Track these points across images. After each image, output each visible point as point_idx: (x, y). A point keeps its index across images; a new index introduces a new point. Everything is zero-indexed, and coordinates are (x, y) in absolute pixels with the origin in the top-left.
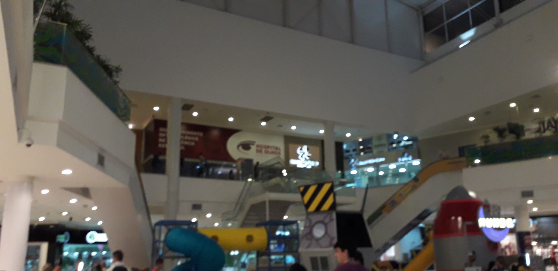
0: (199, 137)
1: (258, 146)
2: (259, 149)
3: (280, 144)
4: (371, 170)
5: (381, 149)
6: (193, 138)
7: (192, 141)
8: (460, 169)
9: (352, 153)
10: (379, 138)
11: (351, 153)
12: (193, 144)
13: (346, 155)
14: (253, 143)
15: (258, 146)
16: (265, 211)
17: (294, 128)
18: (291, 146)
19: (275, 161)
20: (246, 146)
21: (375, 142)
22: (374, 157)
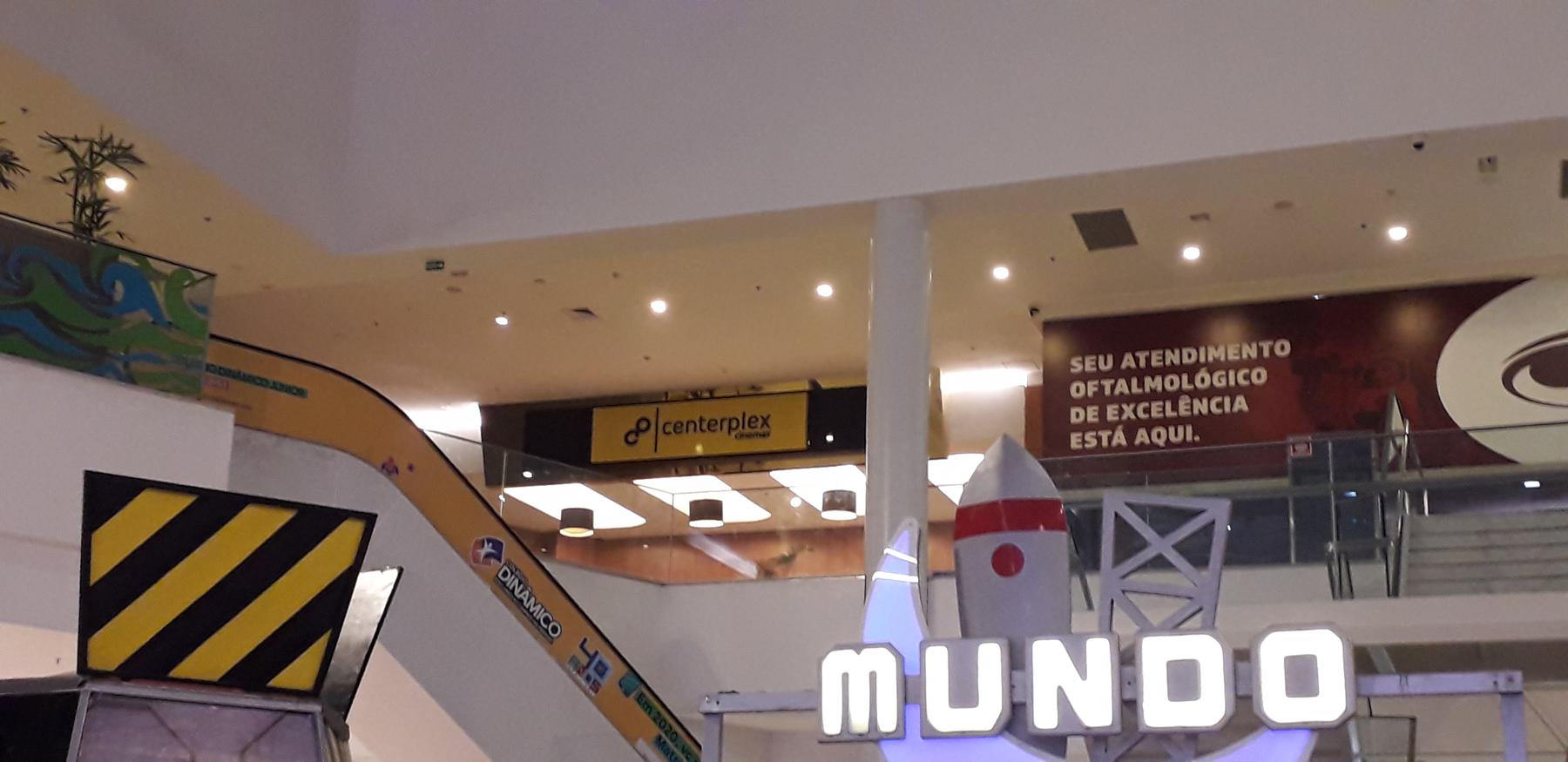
0: (1271, 363)
7: (1232, 392)
12: (1241, 404)
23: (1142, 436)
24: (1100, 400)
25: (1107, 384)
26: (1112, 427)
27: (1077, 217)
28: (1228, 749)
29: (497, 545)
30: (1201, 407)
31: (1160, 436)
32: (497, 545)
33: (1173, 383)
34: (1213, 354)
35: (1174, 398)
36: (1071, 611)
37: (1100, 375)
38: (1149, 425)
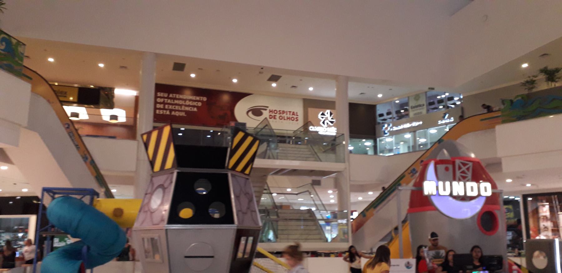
0: (202, 102)
1: (270, 111)
2: (273, 114)
3: (298, 108)
4: (408, 136)
5: (418, 111)
6: (195, 104)
7: (194, 106)
8: (493, 127)
9: (385, 117)
10: (417, 97)
11: (385, 117)
12: (195, 109)
13: (379, 119)
14: (265, 108)
15: (270, 111)
16: (10, 219)
17: (311, 89)
18: (311, 111)
19: (261, 126)
20: (257, 112)
21: (412, 103)
22: (411, 122)
23: (173, 113)
24: (164, 103)
25: (166, 100)
26: (166, 110)
27: (281, 77)
28: (229, 265)
29: (69, 125)
30: (187, 109)
31: (177, 114)
32: (69, 125)
33: (181, 102)
34: (181, 97)
35: (181, 105)
36: (399, 154)
37: (164, 98)
38: (175, 111)
